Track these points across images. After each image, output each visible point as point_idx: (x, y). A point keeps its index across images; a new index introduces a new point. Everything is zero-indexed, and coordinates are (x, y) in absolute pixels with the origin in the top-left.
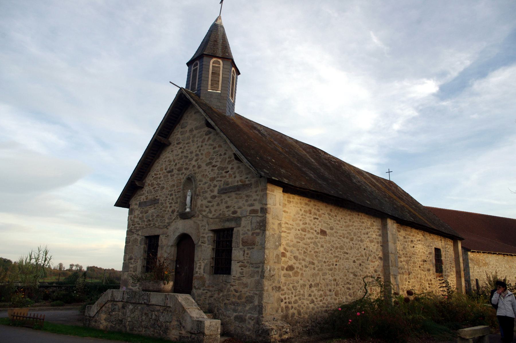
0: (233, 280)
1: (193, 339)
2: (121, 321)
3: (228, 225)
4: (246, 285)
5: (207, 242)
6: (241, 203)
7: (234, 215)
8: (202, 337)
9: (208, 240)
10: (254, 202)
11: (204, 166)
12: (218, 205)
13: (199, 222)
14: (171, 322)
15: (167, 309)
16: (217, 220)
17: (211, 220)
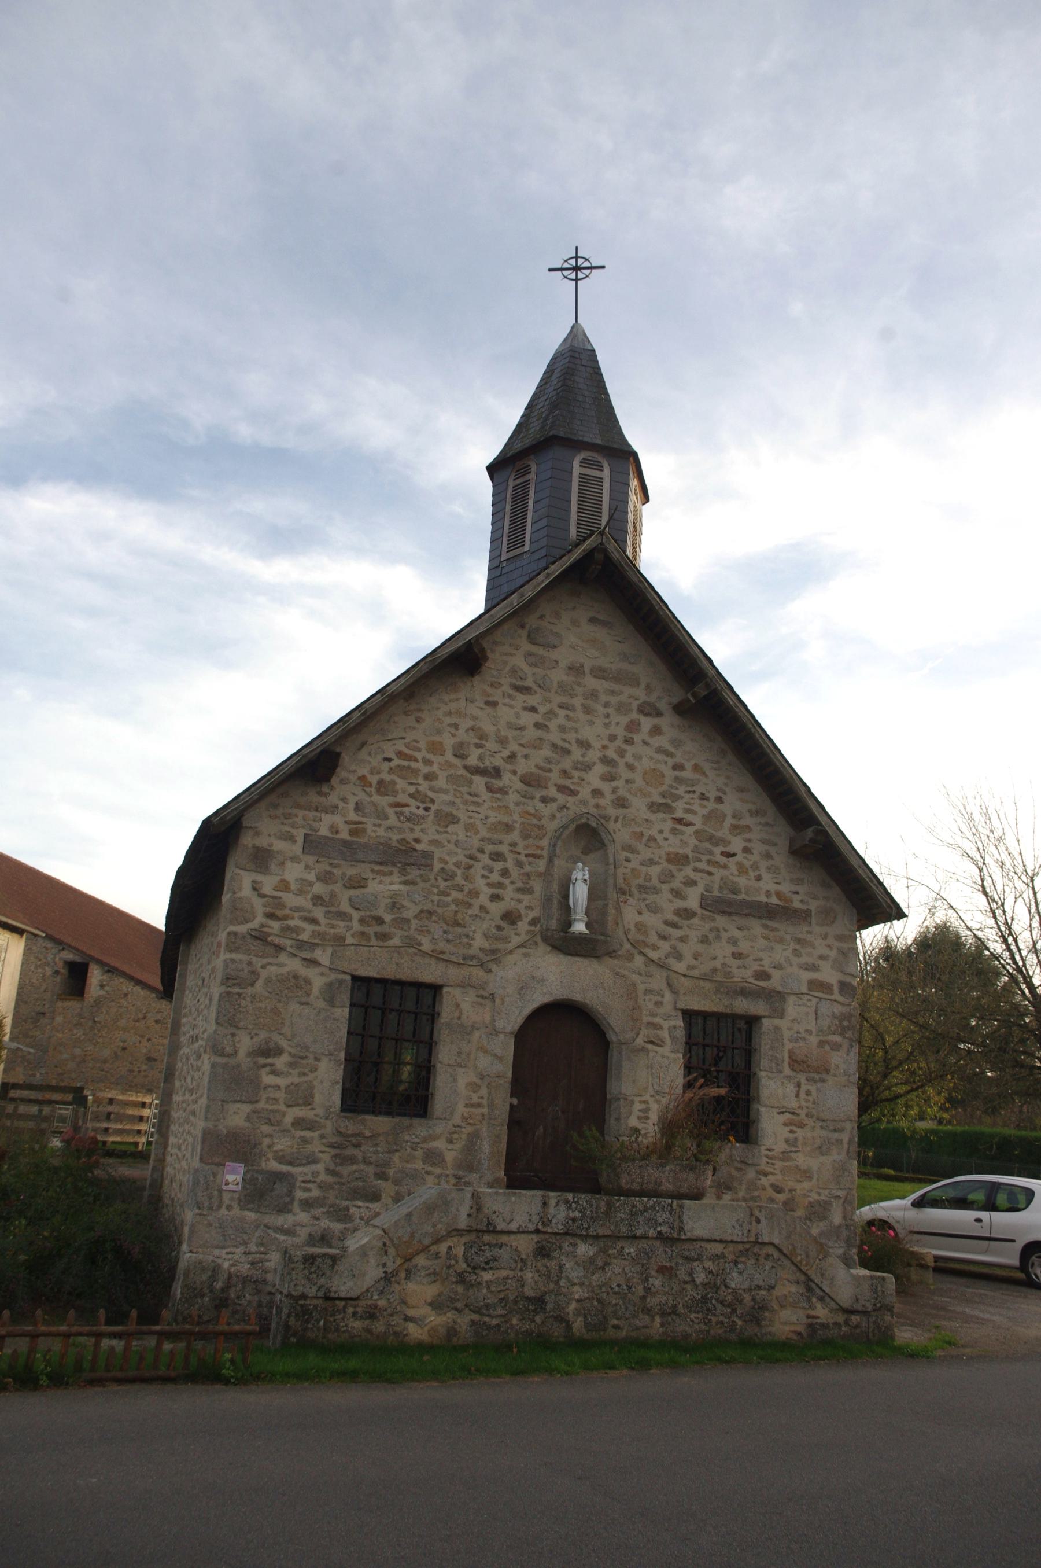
0: (765, 1159)
1: (857, 1327)
2: (539, 1301)
3: (742, 1006)
4: (807, 1174)
5: (668, 1041)
6: (781, 954)
7: (762, 984)
8: (888, 1318)
9: (673, 1038)
10: (820, 962)
11: (639, 806)
12: (704, 940)
13: (635, 977)
14: (772, 1288)
15: (756, 1249)
16: (708, 985)
17: (686, 982)
